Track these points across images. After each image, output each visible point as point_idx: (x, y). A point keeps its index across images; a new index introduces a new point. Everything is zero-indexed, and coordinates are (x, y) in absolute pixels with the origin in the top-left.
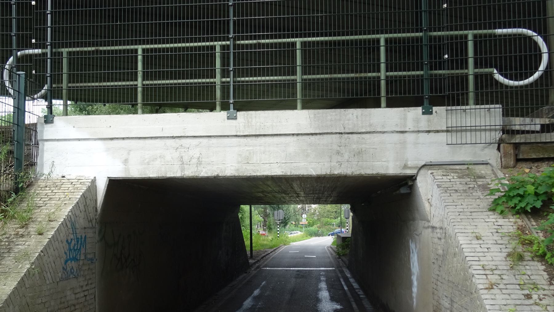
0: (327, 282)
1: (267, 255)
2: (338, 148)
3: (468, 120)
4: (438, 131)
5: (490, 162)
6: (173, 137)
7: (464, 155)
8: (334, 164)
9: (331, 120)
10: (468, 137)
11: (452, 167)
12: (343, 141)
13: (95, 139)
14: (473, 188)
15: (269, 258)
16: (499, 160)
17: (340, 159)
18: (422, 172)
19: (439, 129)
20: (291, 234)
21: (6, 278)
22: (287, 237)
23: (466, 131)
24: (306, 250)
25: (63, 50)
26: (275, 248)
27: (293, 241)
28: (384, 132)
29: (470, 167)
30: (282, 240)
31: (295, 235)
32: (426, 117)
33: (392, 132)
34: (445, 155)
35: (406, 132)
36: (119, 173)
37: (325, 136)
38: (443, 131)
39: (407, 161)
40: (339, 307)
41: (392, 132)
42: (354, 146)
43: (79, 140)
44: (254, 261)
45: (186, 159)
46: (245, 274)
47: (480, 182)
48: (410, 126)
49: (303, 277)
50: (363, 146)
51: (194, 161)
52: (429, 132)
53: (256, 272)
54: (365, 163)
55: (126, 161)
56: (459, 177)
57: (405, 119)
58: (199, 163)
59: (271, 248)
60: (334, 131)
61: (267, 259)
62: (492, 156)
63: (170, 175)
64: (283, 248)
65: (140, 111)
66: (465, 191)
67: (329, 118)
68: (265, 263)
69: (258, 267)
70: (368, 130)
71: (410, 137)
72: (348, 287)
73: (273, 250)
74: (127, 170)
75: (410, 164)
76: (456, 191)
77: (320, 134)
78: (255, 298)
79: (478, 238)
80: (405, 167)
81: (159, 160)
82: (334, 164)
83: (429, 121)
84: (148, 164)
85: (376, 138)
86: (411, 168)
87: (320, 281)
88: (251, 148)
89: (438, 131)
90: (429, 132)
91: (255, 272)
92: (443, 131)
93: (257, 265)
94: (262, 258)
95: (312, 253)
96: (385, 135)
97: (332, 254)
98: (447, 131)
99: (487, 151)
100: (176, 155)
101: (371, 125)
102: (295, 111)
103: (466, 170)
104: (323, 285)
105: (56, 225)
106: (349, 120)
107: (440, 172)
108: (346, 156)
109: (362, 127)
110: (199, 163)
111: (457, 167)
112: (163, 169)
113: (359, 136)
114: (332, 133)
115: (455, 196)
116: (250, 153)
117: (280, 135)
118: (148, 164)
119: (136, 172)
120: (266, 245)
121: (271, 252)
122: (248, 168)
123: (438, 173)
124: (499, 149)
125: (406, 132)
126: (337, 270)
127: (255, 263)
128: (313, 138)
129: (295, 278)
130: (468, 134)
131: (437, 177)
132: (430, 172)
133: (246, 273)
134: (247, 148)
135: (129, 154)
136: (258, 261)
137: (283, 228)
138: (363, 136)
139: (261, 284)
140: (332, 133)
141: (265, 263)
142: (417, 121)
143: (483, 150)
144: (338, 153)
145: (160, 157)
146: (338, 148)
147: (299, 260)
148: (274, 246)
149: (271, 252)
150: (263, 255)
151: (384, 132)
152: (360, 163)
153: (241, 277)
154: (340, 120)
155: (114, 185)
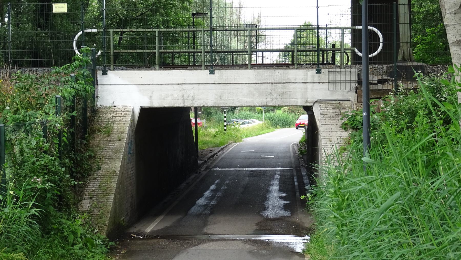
0: (280, 180)
1: (214, 155)
2: (271, 91)
3: (339, 77)
4: (324, 83)
5: (351, 99)
6: (178, 84)
7: (337, 96)
8: (268, 100)
9: (267, 76)
10: (340, 86)
11: (331, 102)
12: (273, 87)
13: (133, 85)
14: (338, 115)
15: (217, 158)
16: (356, 98)
17: (272, 97)
18: (316, 104)
19: (325, 81)
20: (243, 123)
21: (115, 161)
22: (238, 131)
23: (338, 82)
24: (263, 149)
25: (110, 30)
26: (223, 146)
27: (247, 136)
28: (295, 83)
29: (340, 102)
30: (231, 135)
31: (250, 125)
32: (318, 74)
33: (300, 83)
34: (327, 95)
35: (307, 83)
36: (147, 104)
37: (264, 84)
38: (327, 83)
39: (308, 98)
40: (288, 202)
41: (300, 83)
42: (280, 90)
43: (123, 85)
44: (202, 162)
45: (186, 96)
46: (196, 175)
47: (343, 111)
48: (309, 80)
49: (256, 176)
50: (284, 90)
51: (191, 97)
52: (319, 83)
53: (206, 172)
54: (285, 99)
55: (151, 97)
56: (333, 109)
57: (307, 76)
58: (193, 99)
59: (217, 146)
60: (269, 82)
61: (215, 160)
62: (352, 96)
63: (177, 105)
64: (233, 146)
65: (157, 68)
66: (333, 116)
67: (266, 74)
68: (215, 164)
69: (207, 168)
70: (287, 82)
71: (309, 86)
72: (298, 182)
73: (220, 149)
74: (151, 102)
75: (309, 100)
76: (329, 116)
77: (261, 83)
78: (212, 191)
79: (330, 141)
80: (307, 102)
81: (170, 97)
82: (268, 100)
83: (319, 77)
84: (164, 99)
85: (292, 86)
86: (309, 102)
87: (274, 179)
88: (222, 91)
89: (324, 83)
90: (319, 83)
91: (205, 173)
92: (327, 83)
93: (205, 166)
94: (210, 158)
95: (271, 152)
96: (296, 84)
97: (295, 153)
98: (329, 83)
99: (350, 93)
100: (180, 94)
101: (288, 79)
102: (248, 70)
103: (337, 104)
104: (276, 182)
105: (126, 135)
106: (276, 76)
107: (324, 105)
108: (275, 95)
109: (284, 80)
110: (193, 99)
111: (334, 102)
112: (172, 102)
113: (282, 84)
114: (267, 83)
115: (327, 119)
116: (222, 94)
117: (239, 83)
118: (164, 99)
119: (157, 104)
120: (210, 142)
121: (219, 152)
122: (221, 102)
123: (323, 105)
124: (356, 92)
125: (307, 83)
126: (294, 170)
127: (203, 164)
128: (257, 85)
129: (248, 177)
130: (340, 84)
131: (321, 108)
132: (319, 105)
133: (197, 173)
134: (220, 91)
135: (152, 93)
136: (206, 161)
137: (230, 114)
138: (285, 84)
139: (215, 182)
140: (267, 83)
141: (215, 164)
142: (313, 77)
143: (348, 93)
144: (271, 94)
145: (171, 95)
146: (271, 91)
147: (254, 160)
148: (221, 143)
149: (219, 152)
150: (210, 155)
151: (295, 83)
152: (283, 100)
153: (193, 177)
154: (272, 76)
155: (143, 110)
